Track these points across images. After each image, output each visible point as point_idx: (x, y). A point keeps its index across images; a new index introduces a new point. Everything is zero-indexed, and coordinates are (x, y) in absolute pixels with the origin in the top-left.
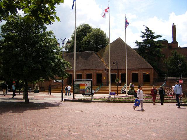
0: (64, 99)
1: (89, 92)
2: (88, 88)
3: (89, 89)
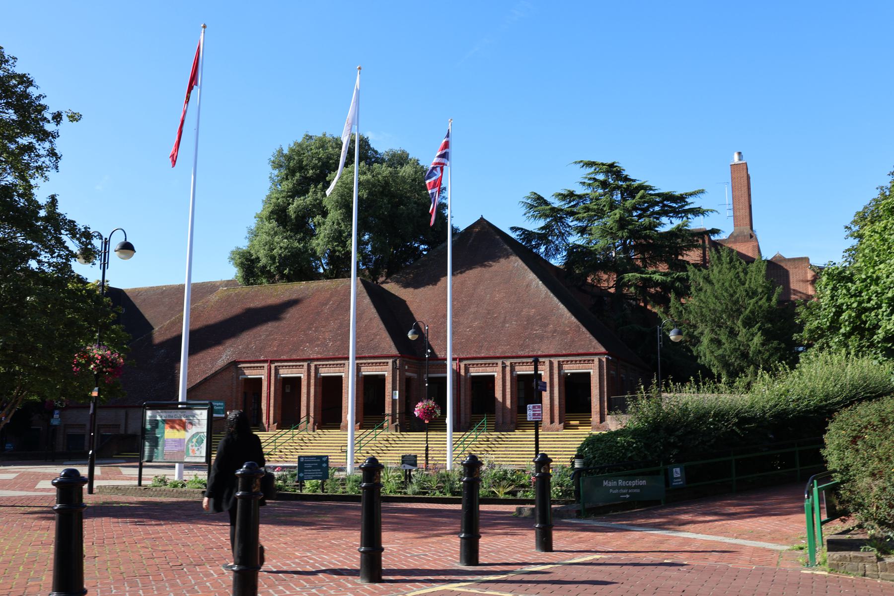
0: (143, 483)
1: (198, 453)
2: (194, 440)
3: (199, 442)
